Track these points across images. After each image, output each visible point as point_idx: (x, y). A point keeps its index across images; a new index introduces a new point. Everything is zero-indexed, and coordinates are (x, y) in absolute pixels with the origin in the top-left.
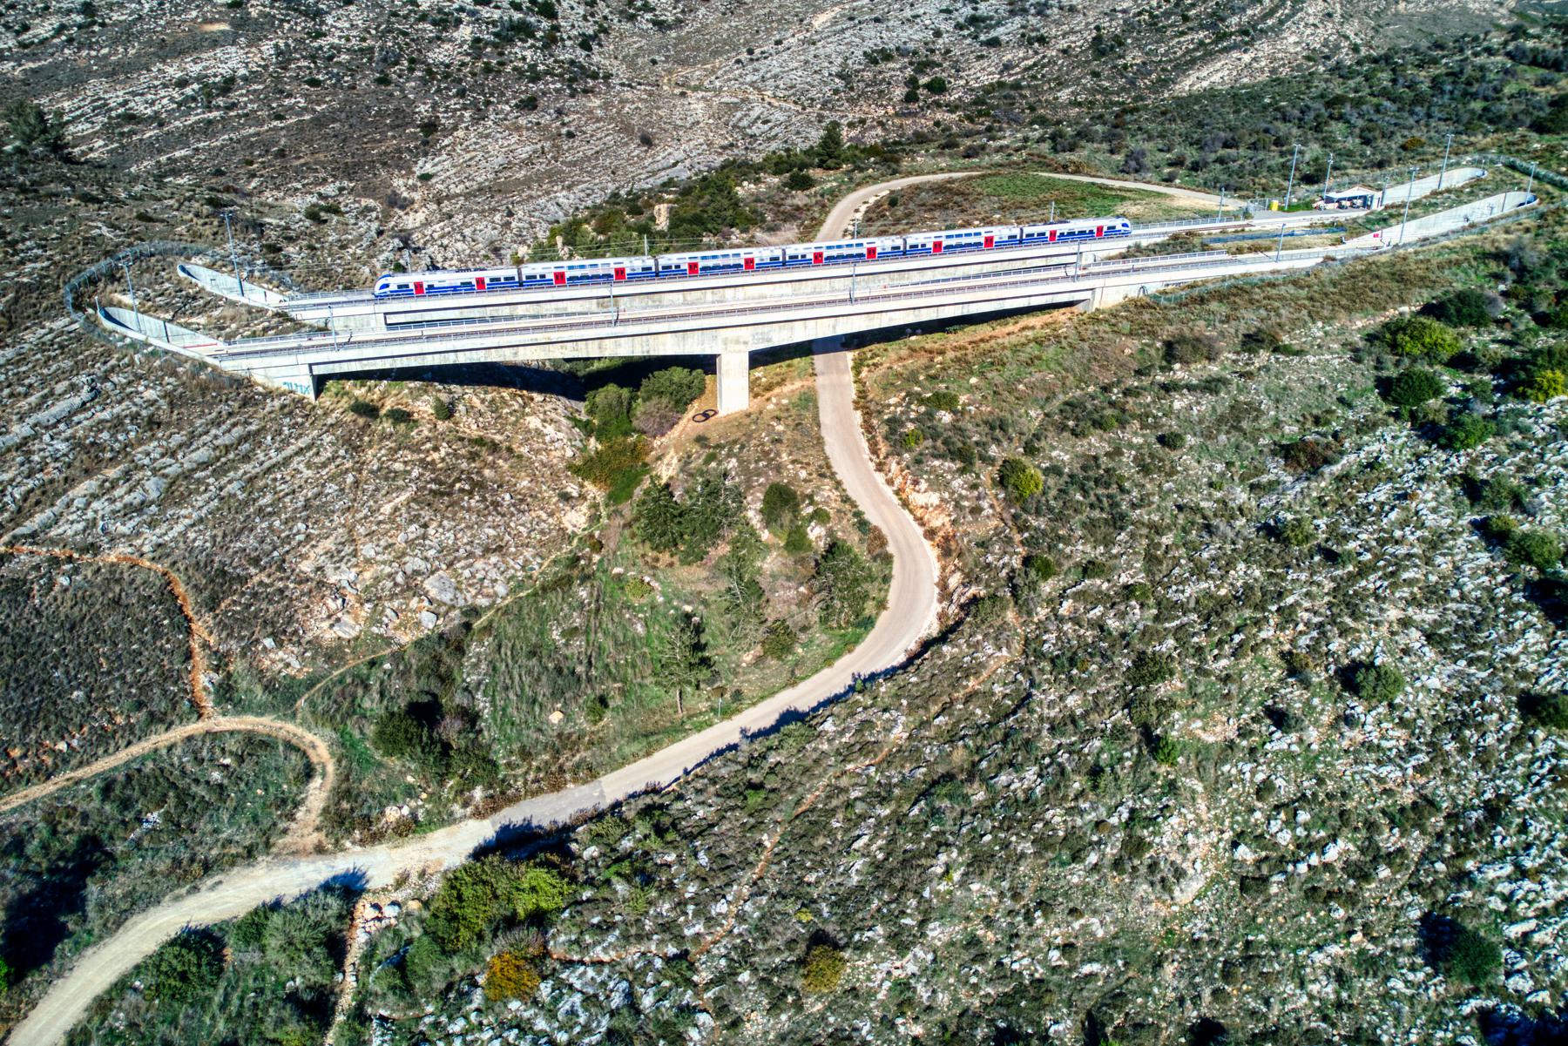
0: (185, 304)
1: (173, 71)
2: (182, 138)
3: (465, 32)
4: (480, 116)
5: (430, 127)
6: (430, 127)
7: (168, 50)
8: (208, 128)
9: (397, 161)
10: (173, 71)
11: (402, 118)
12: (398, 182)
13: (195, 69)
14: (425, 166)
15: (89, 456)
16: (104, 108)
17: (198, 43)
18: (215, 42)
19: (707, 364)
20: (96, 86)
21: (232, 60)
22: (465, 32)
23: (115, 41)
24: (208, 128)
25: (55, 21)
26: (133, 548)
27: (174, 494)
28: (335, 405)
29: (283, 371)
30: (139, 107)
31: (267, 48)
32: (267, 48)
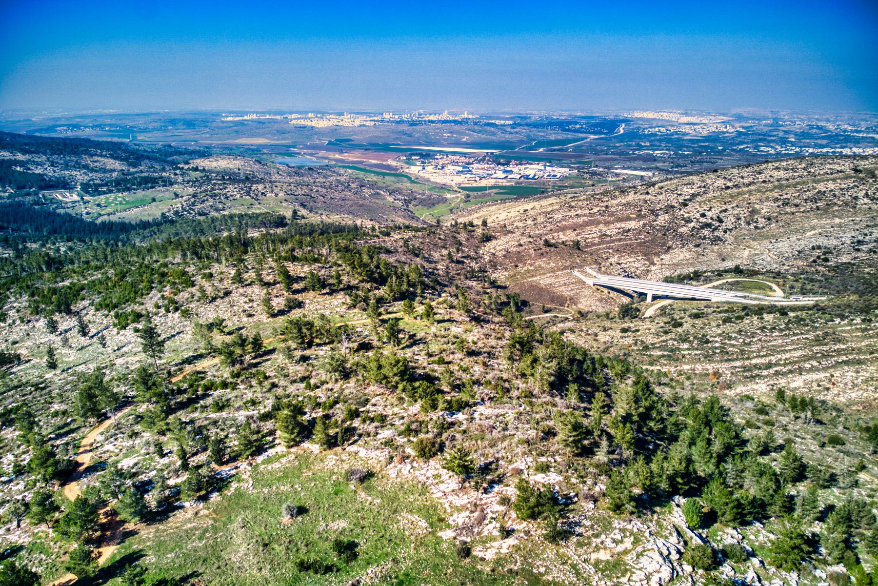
0: (583, 272)
1: (618, 225)
2: (613, 241)
3: (692, 225)
4: (683, 246)
5: (669, 248)
6: (669, 248)
7: (620, 220)
8: (620, 240)
9: (657, 254)
10: (618, 225)
11: (664, 244)
12: (655, 259)
13: (623, 226)
14: (663, 256)
15: (565, 284)
16: (600, 231)
17: (628, 219)
18: (630, 219)
19: (646, 295)
20: (601, 226)
21: (632, 225)
22: (692, 225)
23: (609, 216)
24: (620, 240)
25: (599, 208)
26: (566, 294)
27: (572, 290)
28: (594, 288)
29: (590, 282)
30: (608, 233)
31: (641, 223)
32: (641, 223)
